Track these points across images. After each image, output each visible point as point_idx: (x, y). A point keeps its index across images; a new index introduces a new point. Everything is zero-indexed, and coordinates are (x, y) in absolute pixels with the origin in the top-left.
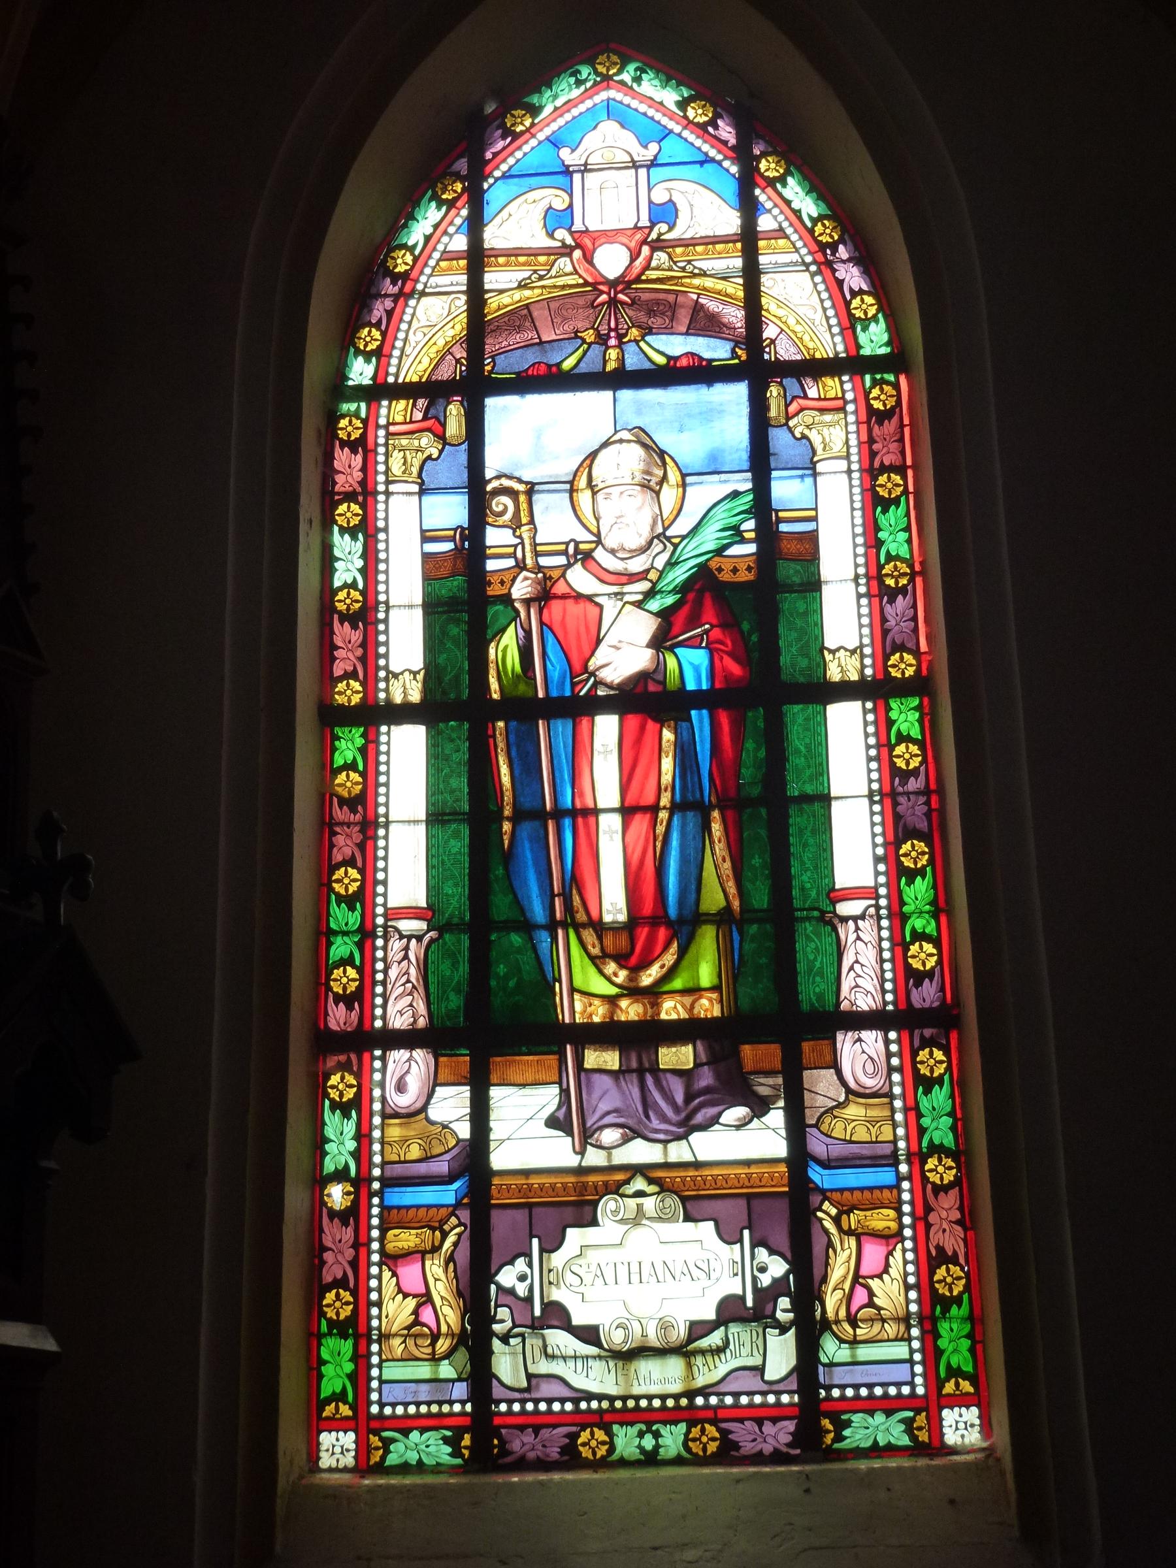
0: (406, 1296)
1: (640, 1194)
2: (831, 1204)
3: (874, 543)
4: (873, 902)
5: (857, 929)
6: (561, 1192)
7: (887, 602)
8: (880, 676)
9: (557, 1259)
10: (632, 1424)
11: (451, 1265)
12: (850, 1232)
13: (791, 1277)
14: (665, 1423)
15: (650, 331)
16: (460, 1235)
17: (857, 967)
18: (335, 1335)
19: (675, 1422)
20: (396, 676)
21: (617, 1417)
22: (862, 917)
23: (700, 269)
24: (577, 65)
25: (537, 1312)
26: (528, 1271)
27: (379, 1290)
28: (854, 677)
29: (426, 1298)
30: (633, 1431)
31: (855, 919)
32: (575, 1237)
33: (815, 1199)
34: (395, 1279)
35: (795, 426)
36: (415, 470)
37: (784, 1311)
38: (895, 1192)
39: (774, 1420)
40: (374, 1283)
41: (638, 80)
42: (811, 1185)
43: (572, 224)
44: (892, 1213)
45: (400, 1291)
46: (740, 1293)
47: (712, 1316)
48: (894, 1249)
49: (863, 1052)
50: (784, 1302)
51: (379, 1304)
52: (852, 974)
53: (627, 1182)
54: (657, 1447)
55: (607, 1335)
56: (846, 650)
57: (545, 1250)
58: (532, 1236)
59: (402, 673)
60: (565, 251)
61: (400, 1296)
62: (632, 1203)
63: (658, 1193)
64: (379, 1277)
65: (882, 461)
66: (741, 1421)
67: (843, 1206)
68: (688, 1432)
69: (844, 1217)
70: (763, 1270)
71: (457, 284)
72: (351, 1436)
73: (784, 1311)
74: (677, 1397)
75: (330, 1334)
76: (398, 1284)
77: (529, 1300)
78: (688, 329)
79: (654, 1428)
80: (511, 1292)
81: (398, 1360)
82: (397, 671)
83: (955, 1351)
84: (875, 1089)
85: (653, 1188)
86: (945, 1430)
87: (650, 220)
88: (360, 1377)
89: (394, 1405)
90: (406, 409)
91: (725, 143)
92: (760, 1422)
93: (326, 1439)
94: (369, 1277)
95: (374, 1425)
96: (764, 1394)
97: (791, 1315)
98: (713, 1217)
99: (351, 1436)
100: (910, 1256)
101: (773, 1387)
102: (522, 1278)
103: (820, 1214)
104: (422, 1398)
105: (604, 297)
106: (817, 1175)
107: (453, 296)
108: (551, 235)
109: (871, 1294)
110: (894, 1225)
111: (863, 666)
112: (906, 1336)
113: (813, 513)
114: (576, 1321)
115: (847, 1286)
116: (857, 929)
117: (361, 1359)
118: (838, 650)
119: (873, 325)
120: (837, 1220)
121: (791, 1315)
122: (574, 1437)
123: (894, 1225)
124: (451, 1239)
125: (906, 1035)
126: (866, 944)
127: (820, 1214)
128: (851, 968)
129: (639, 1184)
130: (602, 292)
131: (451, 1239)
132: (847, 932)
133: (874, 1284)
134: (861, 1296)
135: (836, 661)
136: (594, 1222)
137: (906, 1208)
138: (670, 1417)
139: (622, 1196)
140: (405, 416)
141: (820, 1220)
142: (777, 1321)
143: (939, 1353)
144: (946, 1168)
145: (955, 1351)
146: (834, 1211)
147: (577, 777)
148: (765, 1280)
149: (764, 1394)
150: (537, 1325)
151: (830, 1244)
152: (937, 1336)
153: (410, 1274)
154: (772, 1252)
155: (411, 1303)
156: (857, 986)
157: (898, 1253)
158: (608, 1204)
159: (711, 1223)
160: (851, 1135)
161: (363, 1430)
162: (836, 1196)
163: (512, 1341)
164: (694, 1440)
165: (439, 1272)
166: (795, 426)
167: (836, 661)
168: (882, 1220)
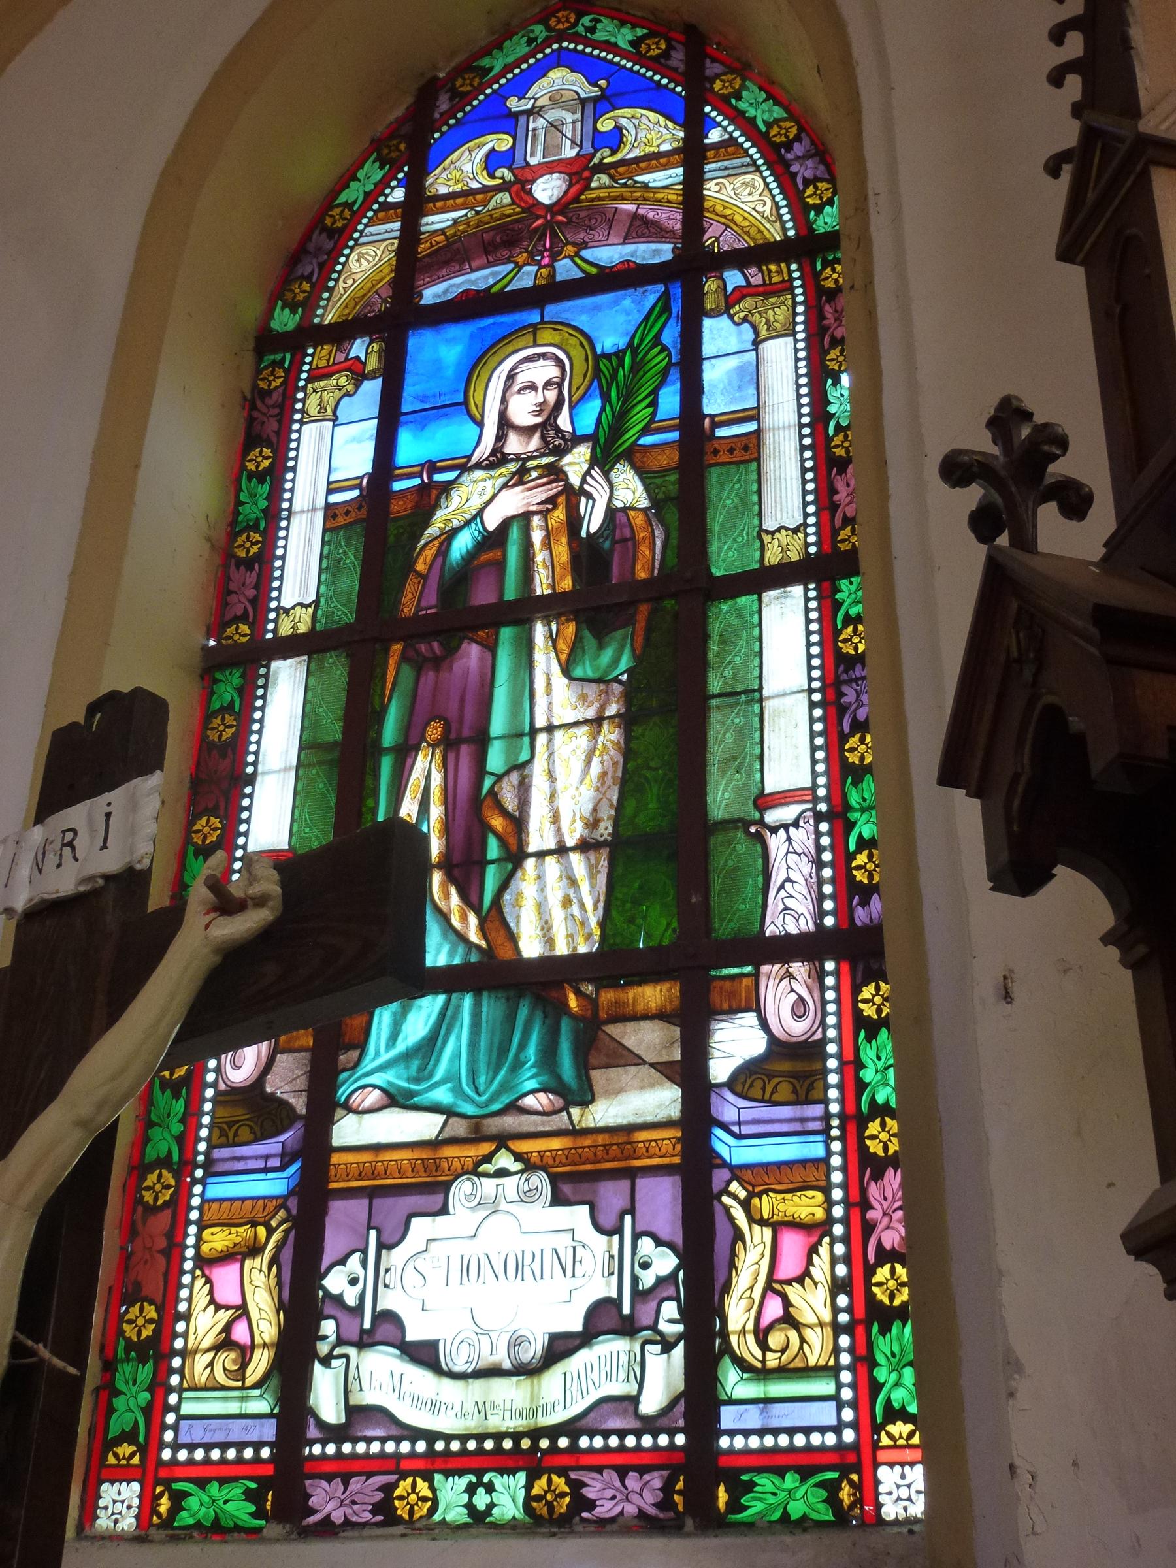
0: (218, 1307)
1: (502, 1173)
2: (741, 1185)
3: (819, 401)
4: (810, 806)
5: (789, 839)
6: (409, 1173)
7: (836, 474)
8: (804, 232)
9: (396, 1257)
10: (461, 1473)
11: (275, 1269)
12: (763, 1222)
13: (681, 1274)
14: (502, 1472)
15: (584, 245)
16: (287, 1232)
17: (788, 885)
18: (133, 1360)
19: (512, 1472)
20: (287, 612)
21: (439, 1464)
22: (795, 824)
23: (643, 182)
24: (531, 25)
25: (367, 1325)
26: (361, 1272)
27: (190, 1300)
28: (794, 556)
29: (242, 1311)
30: (463, 1482)
31: (786, 827)
32: (421, 1227)
33: (719, 1177)
34: (208, 1286)
35: (736, 313)
36: (329, 412)
37: (671, 1321)
38: (823, 1167)
39: (642, 1470)
40: (184, 1293)
41: (592, 30)
42: (718, 1161)
43: (514, 161)
44: (819, 1196)
45: (212, 1301)
46: (614, 1295)
47: (577, 1326)
48: (819, 1243)
49: (792, 990)
50: (670, 1309)
51: (187, 1316)
52: (782, 893)
53: (488, 1159)
54: (491, 1506)
55: (448, 1359)
56: (787, 529)
57: (382, 1246)
58: (369, 1228)
59: (293, 608)
60: (504, 187)
61: (212, 1308)
62: (489, 1185)
63: (522, 1172)
64: (191, 1287)
65: (845, 514)
66: (599, 1470)
67: (754, 1186)
68: (528, 1487)
69: (756, 1201)
70: (645, 1266)
71: (392, 231)
72: (136, 1487)
73: (671, 1321)
74: (516, 1437)
75: (128, 1359)
76: (211, 1292)
77: (358, 1310)
78: (625, 239)
79: (486, 1479)
80: (338, 1300)
81: (205, 1389)
82: (288, 606)
83: (897, 1384)
84: (803, 1038)
85: (518, 1166)
86: (883, 1499)
87: (593, 146)
88: (154, 1411)
89: (192, 1447)
90: (330, 354)
91: (676, 70)
92: (622, 1472)
93: (108, 1492)
94: (181, 1286)
95: (163, 1474)
96: (638, 1434)
97: (680, 1328)
98: (587, 1198)
99: (136, 1487)
100: (840, 1249)
101: (650, 1425)
102: (353, 1282)
103: (726, 1200)
104: (234, 1437)
105: (540, 222)
106: (722, 1143)
107: (387, 243)
108: (492, 176)
109: (787, 1304)
110: (820, 1214)
111: (807, 545)
112: (832, 1363)
113: (754, 412)
114: (410, 1337)
115: (757, 1294)
116: (789, 839)
117: (158, 1387)
118: (778, 530)
119: (828, 209)
120: (746, 1204)
121: (680, 1328)
122: (388, 1489)
123: (820, 1214)
124: (276, 1236)
125: (845, 967)
126: (799, 855)
127: (726, 1200)
128: (782, 887)
129: (504, 1160)
130: (538, 217)
131: (276, 1236)
132: (776, 843)
133: (793, 1292)
134: (774, 1308)
135: (776, 541)
136: (444, 1210)
137: (837, 1194)
138: (506, 1463)
139: (479, 1175)
140: (328, 361)
141: (727, 1209)
142: (660, 1333)
143: (876, 1387)
144: (890, 1135)
145: (897, 1384)
146: (743, 1194)
147: (799, 1374)
148: (647, 1279)
149: (638, 1434)
150: (364, 1342)
151: (739, 1236)
152: (859, 1065)
153: (226, 1278)
154: (659, 1242)
155: (224, 1316)
156: (786, 908)
157: (824, 1250)
158: (462, 1188)
159: (586, 1208)
160: (772, 1093)
161: (150, 1480)
162: (748, 1175)
163: (335, 1363)
164: (538, 1498)
165: (259, 1278)
166: (736, 313)
167: (776, 541)
168: (807, 1206)
